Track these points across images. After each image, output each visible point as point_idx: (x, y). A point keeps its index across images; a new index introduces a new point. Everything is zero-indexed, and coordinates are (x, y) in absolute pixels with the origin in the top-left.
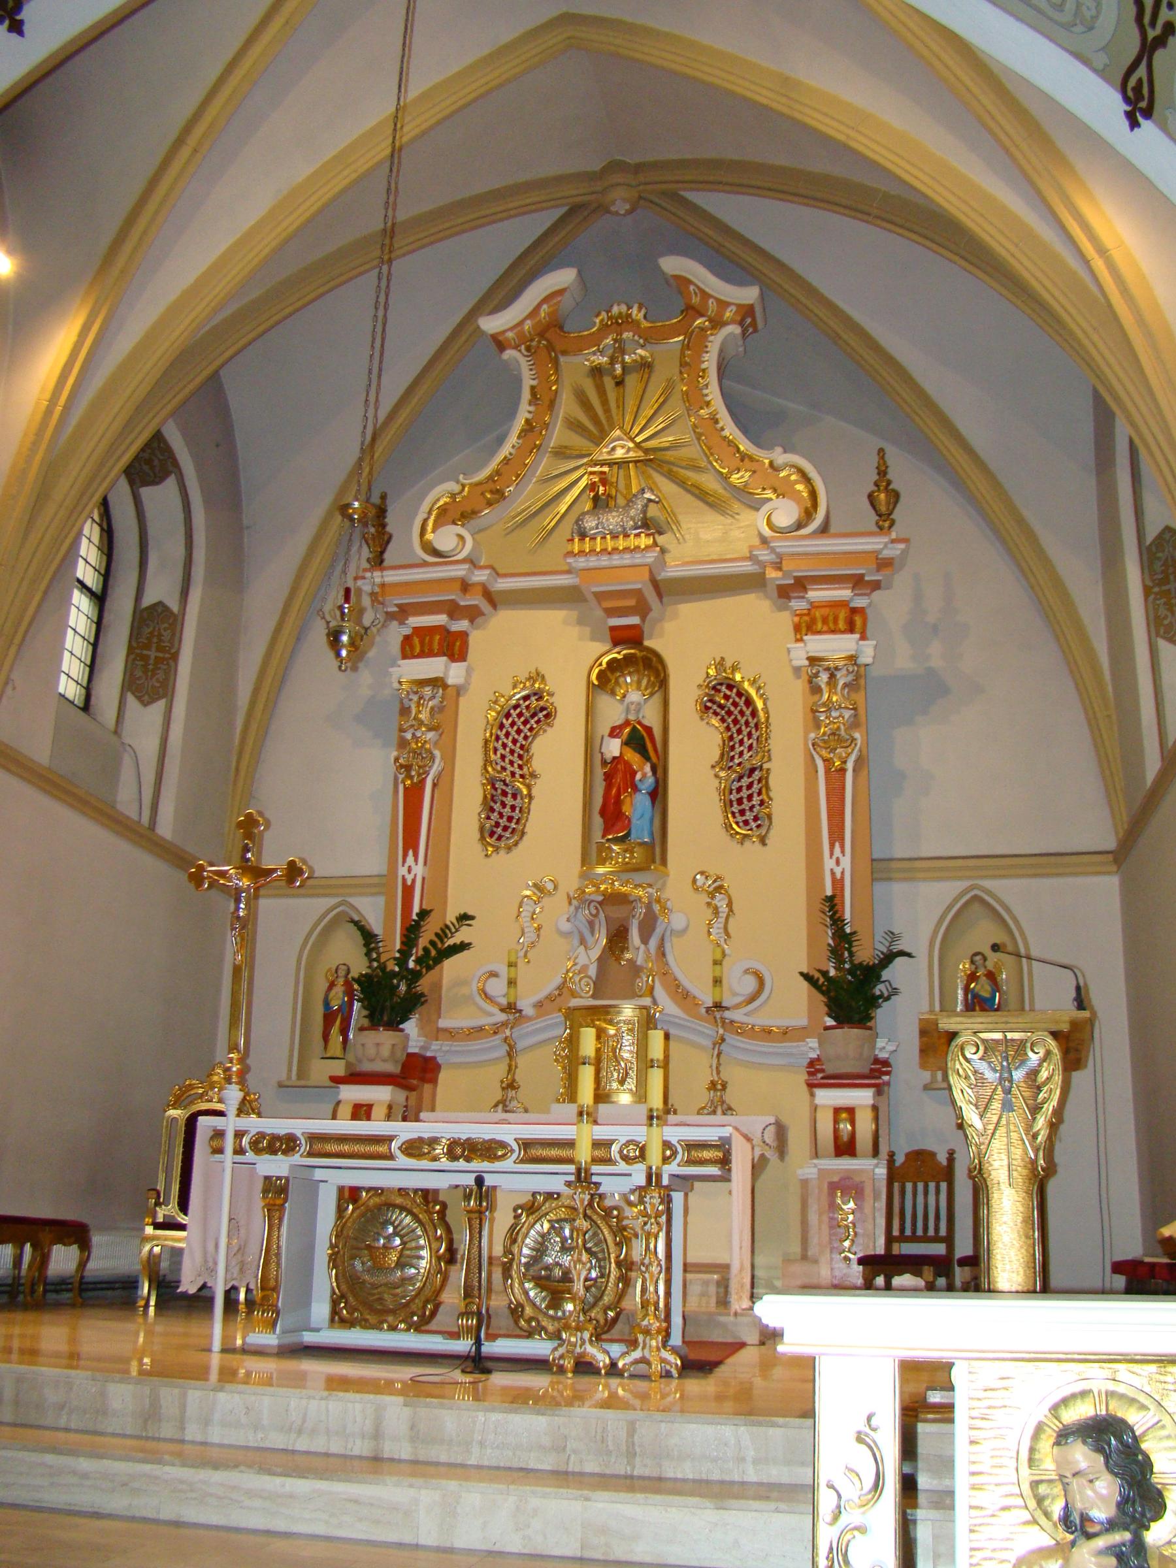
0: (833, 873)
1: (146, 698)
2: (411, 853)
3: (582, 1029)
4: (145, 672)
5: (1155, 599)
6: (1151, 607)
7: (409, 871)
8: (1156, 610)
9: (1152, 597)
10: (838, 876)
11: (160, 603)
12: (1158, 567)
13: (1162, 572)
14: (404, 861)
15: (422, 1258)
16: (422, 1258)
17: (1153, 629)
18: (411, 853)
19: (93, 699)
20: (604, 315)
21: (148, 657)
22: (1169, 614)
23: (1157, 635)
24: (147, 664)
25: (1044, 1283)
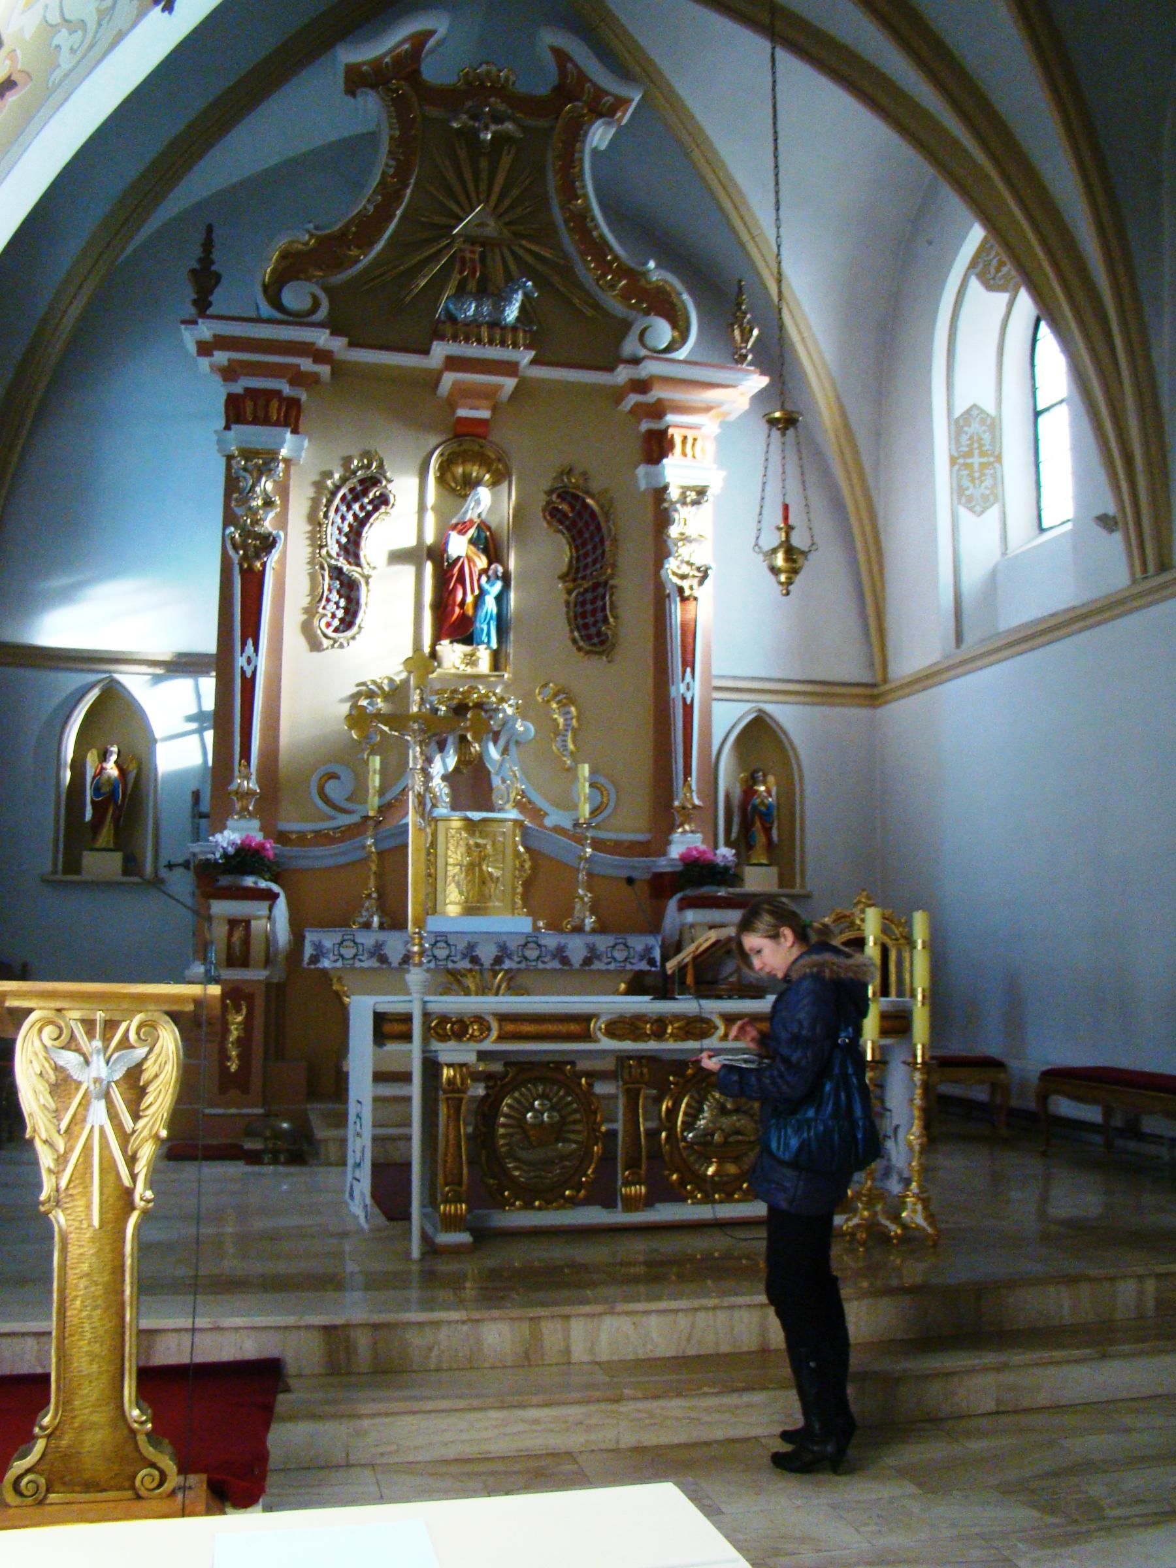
0: (243, 672)
1: (978, 508)
2: (250, 642)
3: (85, 853)
4: (972, 480)
5: (959, 470)
6: (954, 475)
7: (249, 661)
8: (959, 480)
9: (956, 467)
10: (249, 675)
11: (975, 406)
12: (964, 439)
13: (968, 446)
14: (243, 651)
15: (509, 1106)
16: (509, 1106)
17: (955, 496)
18: (250, 642)
19: (760, 489)
20: (494, 69)
21: (972, 464)
22: (971, 486)
23: (959, 503)
24: (972, 471)
25: (376, 1100)
